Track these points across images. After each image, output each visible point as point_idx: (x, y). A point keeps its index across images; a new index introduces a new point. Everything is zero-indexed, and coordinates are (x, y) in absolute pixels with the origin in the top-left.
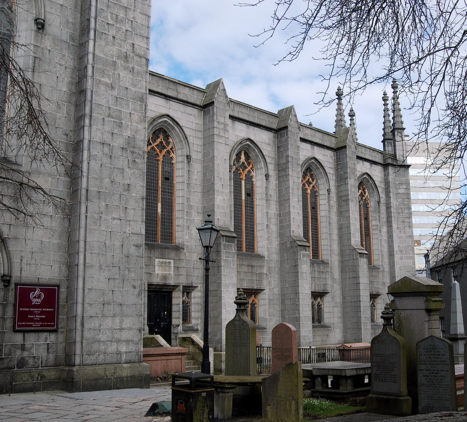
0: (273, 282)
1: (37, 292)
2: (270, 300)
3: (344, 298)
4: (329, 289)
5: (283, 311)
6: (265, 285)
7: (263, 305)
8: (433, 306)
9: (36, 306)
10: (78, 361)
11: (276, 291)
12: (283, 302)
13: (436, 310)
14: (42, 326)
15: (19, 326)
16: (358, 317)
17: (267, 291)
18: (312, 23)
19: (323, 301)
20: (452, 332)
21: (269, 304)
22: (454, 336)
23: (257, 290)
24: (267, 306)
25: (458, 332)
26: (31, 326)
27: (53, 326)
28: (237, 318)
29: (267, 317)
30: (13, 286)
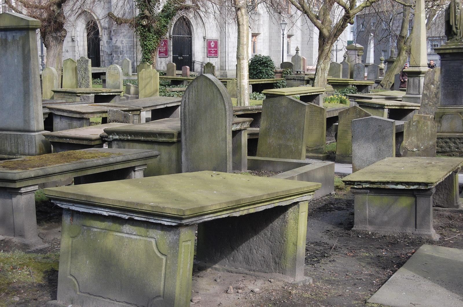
0: (265, 29)
1: (213, 43)
2: (264, 40)
3: (303, 38)
4: (294, 34)
5: (270, 47)
6: (261, 31)
7: (260, 42)
8: (360, 54)
9: (212, 48)
10: (227, 68)
11: (267, 34)
12: (270, 41)
13: (361, 55)
14: (214, 55)
15: (209, 55)
16: (311, 51)
17: (262, 35)
18: (345, 8)
19: (290, 40)
20: (367, 62)
21: (263, 42)
22: (368, 64)
23: (257, 34)
24: (262, 43)
25: (370, 63)
26: (211, 55)
27: (217, 55)
28: (296, 55)
29: (262, 50)
30: (206, 40)
